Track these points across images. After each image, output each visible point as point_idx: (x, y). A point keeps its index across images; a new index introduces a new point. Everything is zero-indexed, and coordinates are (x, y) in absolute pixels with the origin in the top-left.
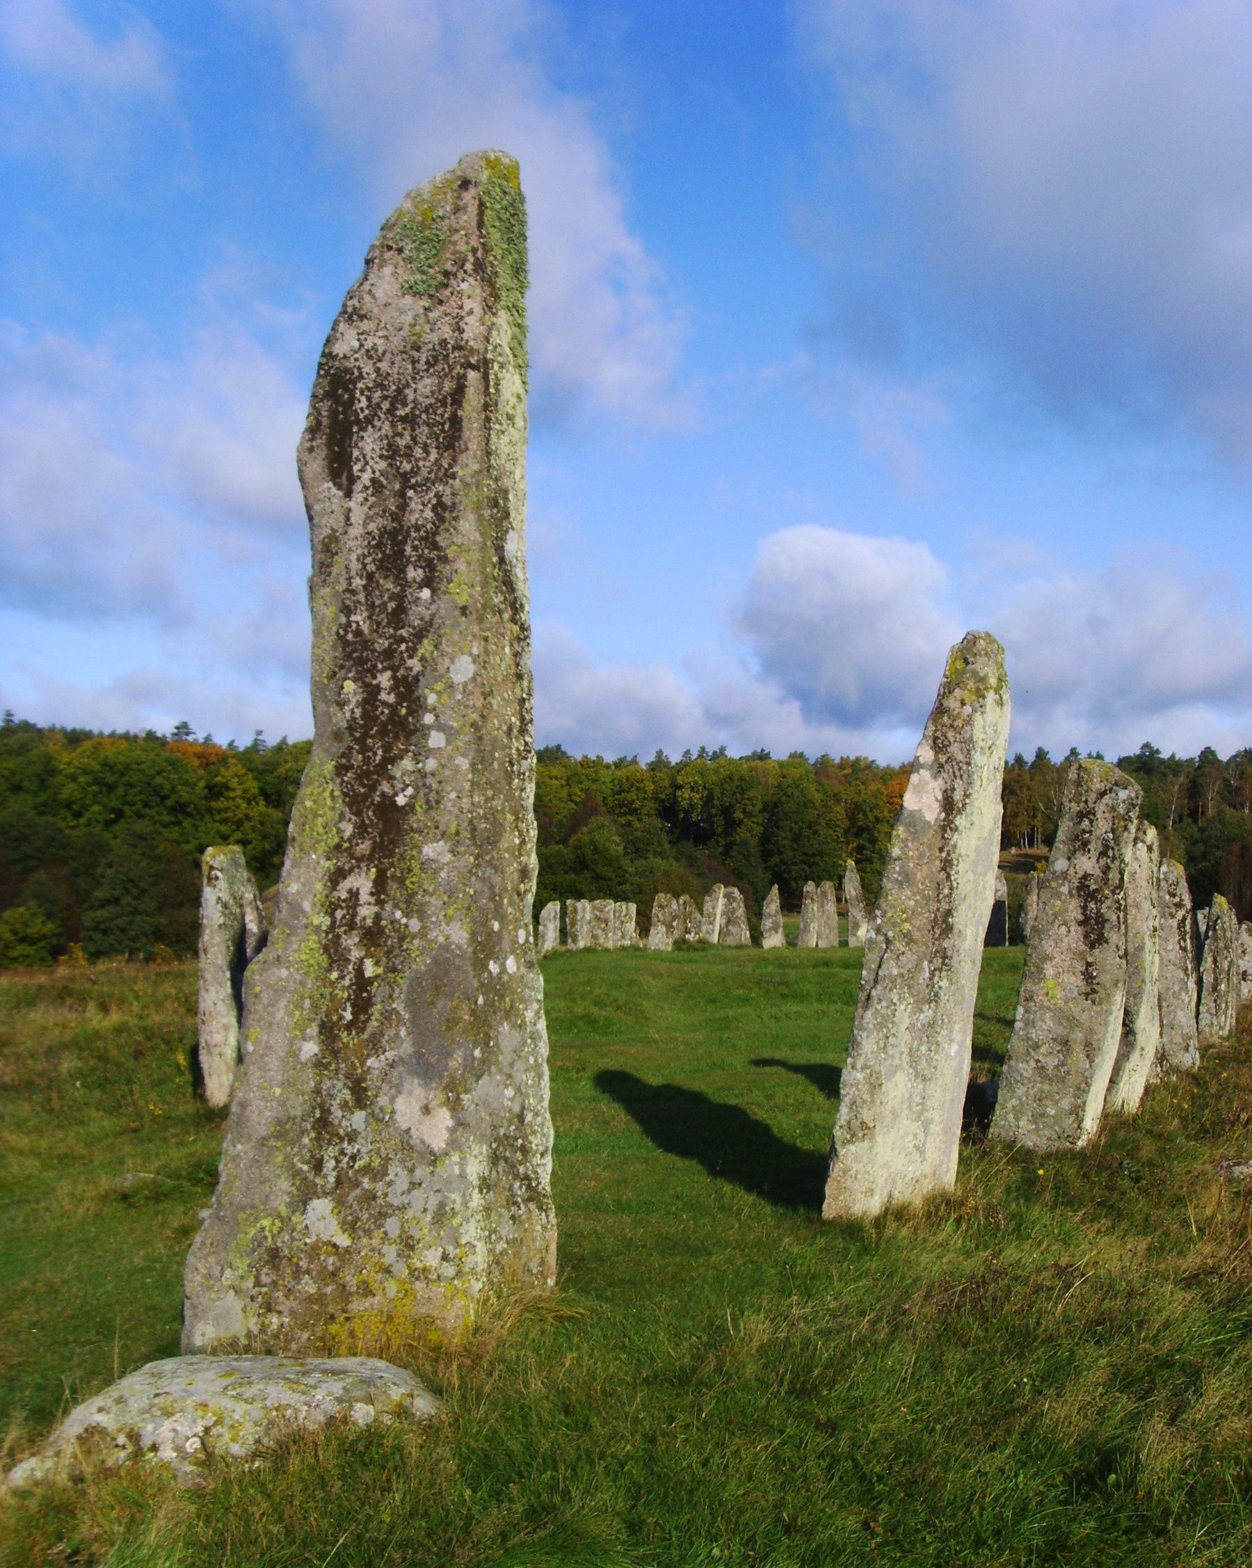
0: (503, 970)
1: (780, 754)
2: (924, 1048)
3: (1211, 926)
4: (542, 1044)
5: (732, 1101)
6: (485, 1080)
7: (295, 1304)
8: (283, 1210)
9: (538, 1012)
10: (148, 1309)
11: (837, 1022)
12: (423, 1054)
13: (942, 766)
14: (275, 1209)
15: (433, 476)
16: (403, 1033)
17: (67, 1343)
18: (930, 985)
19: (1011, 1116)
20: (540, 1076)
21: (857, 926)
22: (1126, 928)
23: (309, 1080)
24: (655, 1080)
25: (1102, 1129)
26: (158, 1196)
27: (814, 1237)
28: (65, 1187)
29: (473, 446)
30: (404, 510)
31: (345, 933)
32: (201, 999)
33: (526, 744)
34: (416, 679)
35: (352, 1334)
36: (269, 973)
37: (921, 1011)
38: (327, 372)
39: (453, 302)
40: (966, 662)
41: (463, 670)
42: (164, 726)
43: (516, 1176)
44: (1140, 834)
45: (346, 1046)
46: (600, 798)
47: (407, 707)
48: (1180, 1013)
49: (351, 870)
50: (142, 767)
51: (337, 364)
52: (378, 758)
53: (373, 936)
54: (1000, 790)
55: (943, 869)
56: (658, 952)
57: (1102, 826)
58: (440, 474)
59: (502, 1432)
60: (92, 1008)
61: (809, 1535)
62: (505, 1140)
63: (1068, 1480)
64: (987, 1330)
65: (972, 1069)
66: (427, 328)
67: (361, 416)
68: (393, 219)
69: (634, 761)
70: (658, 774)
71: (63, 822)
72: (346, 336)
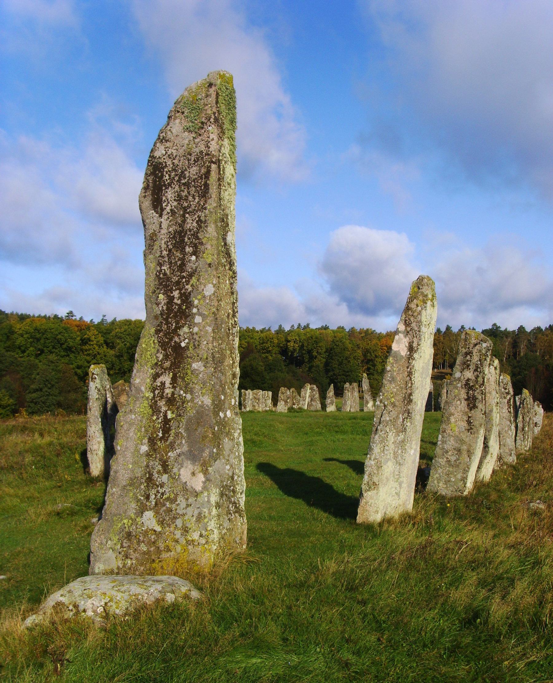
0: (225, 416)
1: (333, 327)
2: (400, 451)
3: (522, 403)
4: (241, 447)
5: (316, 476)
6: (218, 461)
7: (138, 555)
8: (133, 516)
9: (239, 434)
10: (73, 559)
11: (360, 443)
12: (192, 451)
13: (408, 332)
14: (130, 516)
15: (197, 208)
16: (184, 442)
17: (39, 573)
18: (403, 425)
19: (436, 481)
20: (240, 461)
21: (367, 402)
22: (485, 402)
23: (144, 461)
24: (282, 467)
25: (475, 487)
26: (73, 513)
27: (353, 531)
28: (32, 510)
29: (214, 196)
30: (184, 223)
31: (159, 400)
32: (88, 431)
33: (235, 321)
34: (190, 293)
35: (162, 567)
36: (127, 416)
37: (399, 436)
38: (152, 164)
39: (205, 135)
40: (419, 288)
41: (209, 290)
42: (62, 313)
43: (230, 502)
44: (491, 362)
45: (160, 447)
46: (254, 346)
47: (186, 306)
48: (508, 440)
49: (162, 373)
50: (52, 331)
51: (156, 160)
52: (173, 327)
53: (171, 401)
54: (432, 343)
55: (408, 376)
56: (281, 413)
57: (476, 358)
58: (200, 208)
59: (228, 605)
60: (37, 435)
61: (356, 643)
62: (226, 487)
63: (460, 622)
64: (427, 565)
65: (419, 462)
66: (194, 146)
67: (166, 183)
68: (180, 100)
69: (269, 330)
70: (280, 335)
71: (17, 354)
72: (160, 149)
